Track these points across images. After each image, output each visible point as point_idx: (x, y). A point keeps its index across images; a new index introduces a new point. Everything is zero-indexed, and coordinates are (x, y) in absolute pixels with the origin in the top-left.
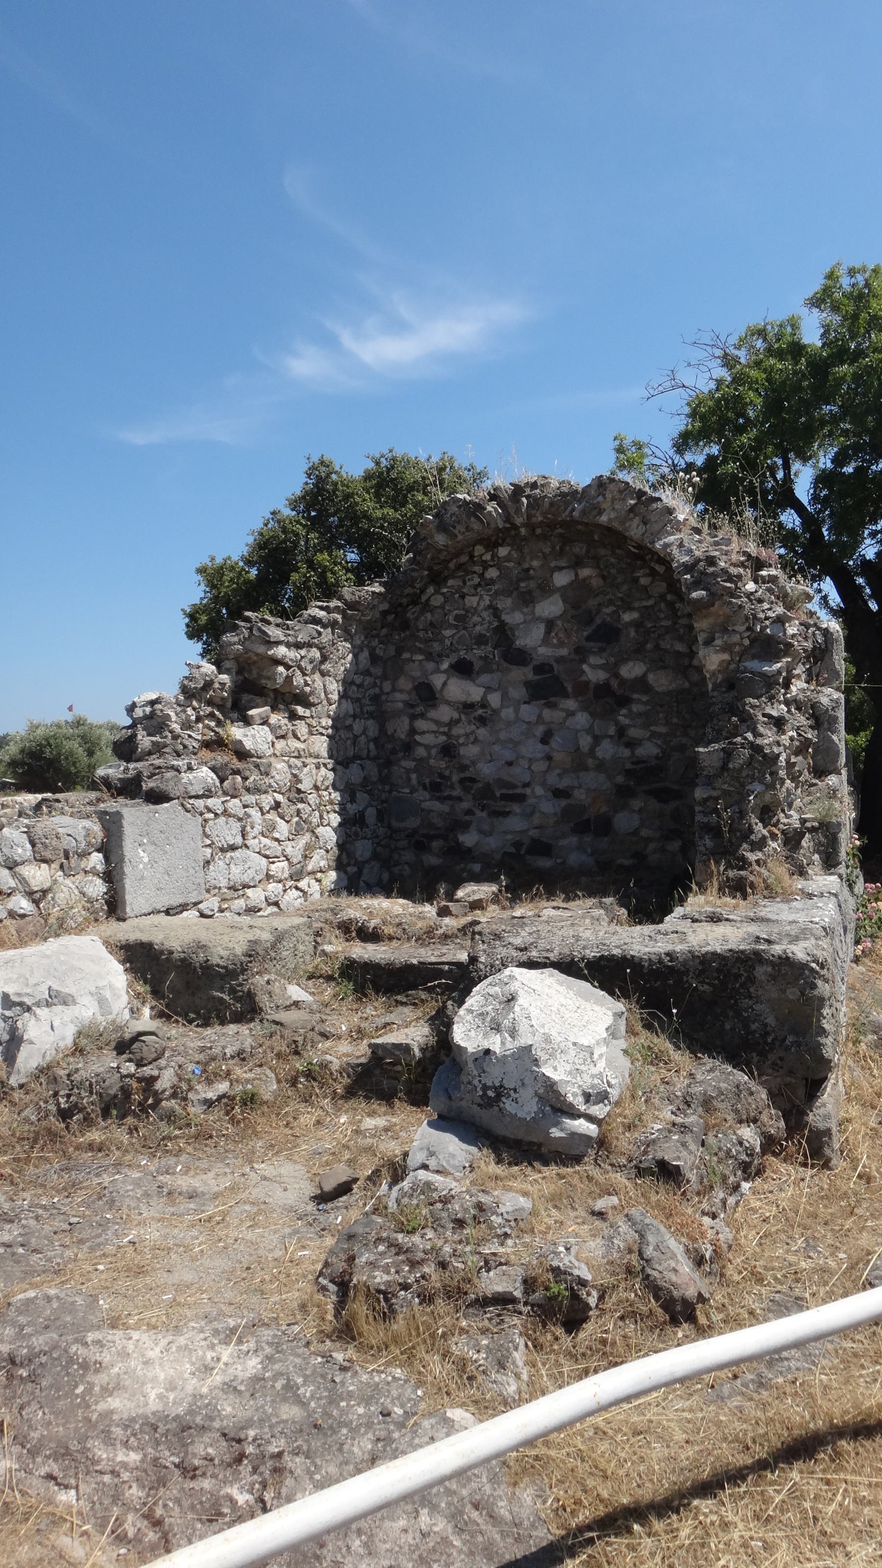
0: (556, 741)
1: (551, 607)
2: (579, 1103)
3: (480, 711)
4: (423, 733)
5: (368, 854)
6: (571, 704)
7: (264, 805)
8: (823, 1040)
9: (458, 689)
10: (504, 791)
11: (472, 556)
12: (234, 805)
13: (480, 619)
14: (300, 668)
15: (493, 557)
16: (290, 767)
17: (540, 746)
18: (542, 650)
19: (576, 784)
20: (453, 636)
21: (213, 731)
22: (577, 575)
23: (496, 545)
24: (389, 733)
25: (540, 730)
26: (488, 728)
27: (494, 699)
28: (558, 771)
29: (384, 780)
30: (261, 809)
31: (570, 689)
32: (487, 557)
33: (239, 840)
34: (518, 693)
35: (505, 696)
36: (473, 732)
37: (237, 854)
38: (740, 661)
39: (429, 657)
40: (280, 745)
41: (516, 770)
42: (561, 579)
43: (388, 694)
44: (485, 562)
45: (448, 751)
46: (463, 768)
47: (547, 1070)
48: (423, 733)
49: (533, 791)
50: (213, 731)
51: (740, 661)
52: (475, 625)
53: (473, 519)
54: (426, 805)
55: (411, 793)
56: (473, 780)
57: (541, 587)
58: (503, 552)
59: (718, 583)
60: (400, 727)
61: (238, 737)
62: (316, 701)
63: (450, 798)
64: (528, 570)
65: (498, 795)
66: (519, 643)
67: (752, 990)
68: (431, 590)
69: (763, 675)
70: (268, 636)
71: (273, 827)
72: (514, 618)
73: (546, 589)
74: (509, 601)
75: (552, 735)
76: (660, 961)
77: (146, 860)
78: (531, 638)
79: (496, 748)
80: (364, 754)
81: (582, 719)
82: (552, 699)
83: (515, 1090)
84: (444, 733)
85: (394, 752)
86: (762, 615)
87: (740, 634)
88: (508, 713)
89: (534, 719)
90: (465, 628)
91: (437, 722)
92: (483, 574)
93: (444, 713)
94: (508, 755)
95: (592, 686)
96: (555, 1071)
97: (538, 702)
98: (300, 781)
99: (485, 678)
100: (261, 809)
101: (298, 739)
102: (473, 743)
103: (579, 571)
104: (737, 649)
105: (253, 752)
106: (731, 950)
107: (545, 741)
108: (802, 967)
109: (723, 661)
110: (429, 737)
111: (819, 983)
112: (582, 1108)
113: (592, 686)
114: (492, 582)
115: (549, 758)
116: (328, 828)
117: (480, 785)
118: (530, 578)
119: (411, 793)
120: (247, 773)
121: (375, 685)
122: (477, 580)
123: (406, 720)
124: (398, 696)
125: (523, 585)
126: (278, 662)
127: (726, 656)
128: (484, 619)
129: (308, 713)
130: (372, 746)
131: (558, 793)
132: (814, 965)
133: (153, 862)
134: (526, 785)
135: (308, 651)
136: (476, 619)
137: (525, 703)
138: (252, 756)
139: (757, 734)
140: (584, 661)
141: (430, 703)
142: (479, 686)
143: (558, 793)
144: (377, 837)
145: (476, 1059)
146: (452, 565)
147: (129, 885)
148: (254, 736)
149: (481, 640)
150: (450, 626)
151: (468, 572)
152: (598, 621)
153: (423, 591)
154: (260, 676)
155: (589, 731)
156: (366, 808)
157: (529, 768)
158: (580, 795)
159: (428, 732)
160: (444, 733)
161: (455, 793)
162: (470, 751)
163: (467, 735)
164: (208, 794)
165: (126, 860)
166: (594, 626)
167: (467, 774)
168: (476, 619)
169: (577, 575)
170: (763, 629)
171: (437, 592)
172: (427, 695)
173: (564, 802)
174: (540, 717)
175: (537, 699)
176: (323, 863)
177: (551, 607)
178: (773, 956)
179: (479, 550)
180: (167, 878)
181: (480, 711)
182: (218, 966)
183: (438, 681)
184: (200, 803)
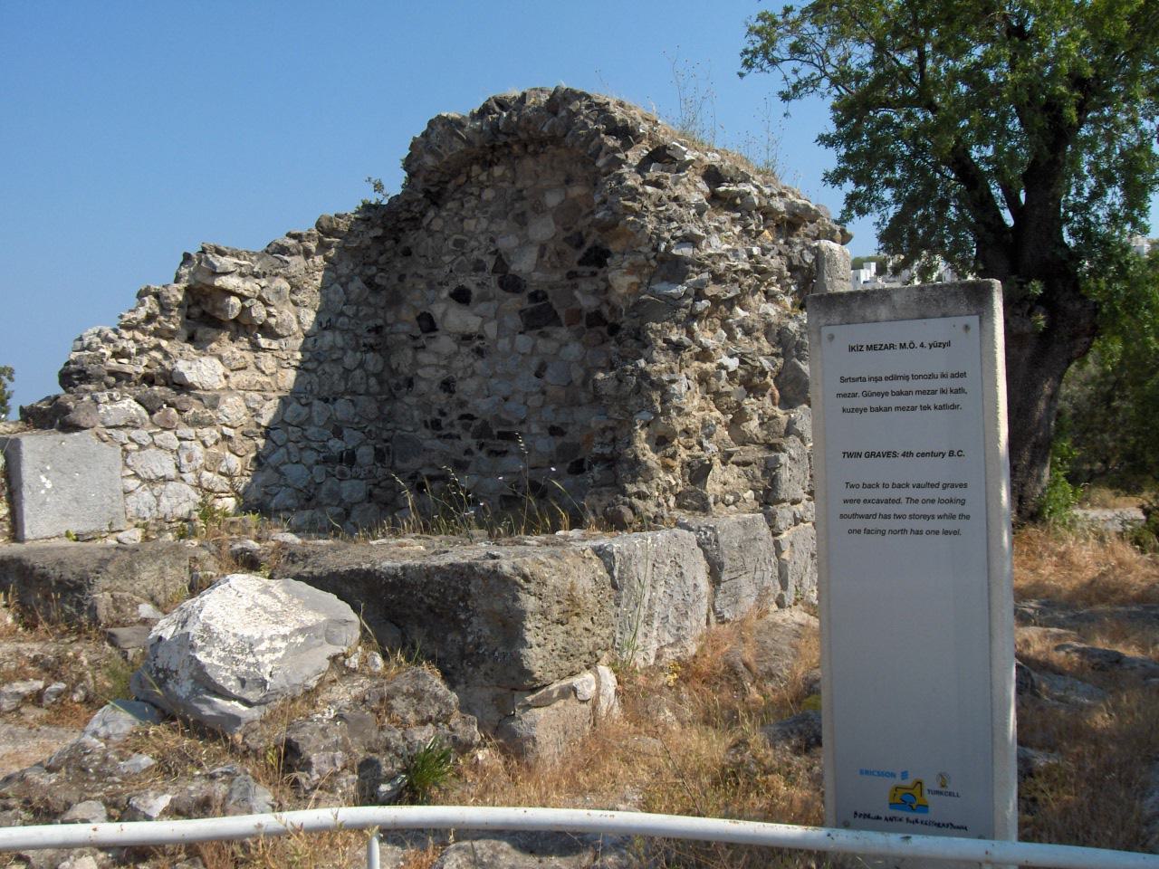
0: (550, 375)
1: (543, 229)
2: (232, 685)
3: (478, 343)
4: (426, 366)
5: (359, 496)
6: (563, 333)
7: (207, 438)
8: (525, 651)
9: (457, 319)
10: (501, 429)
11: (469, 177)
12: (169, 438)
13: (476, 244)
14: (260, 298)
15: (488, 175)
16: (245, 400)
17: (535, 379)
18: (537, 276)
19: (570, 421)
20: (452, 262)
21: (160, 364)
22: (566, 194)
23: (490, 164)
24: (394, 367)
25: (535, 362)
26: (485, 360)
27: (491, 330)
28: (553, 407)
29: (386, 418)
30: (204, 443)
31: (563, 319)
32: (483, 177)
33: (172, 472)
34: (514, 321)
35: (500, 327)
36: (471, 364)
37: (171, 486)
38: (649, 284)
39: (430, 286)
40: (237, 378)
41: (511, 406)
42: (553, 200)
43: (392, 325)
44: (482, 183)
45: (447, 386)
46: (462, 404)
47: (201, 656)
48: (426, 366)
49: (529, 428)
50: (160, 364)
51: (649, 284)
52: (472, 251)
53: (455, 139)
54: (428, 444)
55: (415, 431)
56: (470, 417)
57: (535, 209)
58: (497, 171)
59: (619, 202)
60: (403, 359)
61: (181, 370)
62: (286, 334)
63: (450, 436)
64: (521, 191)
65: (495, 432)
66: (514, 268)
67: (469, 603)
68: (431, 214)
69: (670, 297)
70: (215, 267)
71: (218, 460)
72: (507, 242)
73: (539, 209)
74: (504, 225)
75: (546, 368)
76: (396, 576)
77: (49, 485)
78: (524, 264)
79: (493, 381)
80: (362, 389)
81: (574, 350)
82: (547, 329)
83: (176, 672)
84: (444, 367)
85: (398, 387)
86: (667, 235)
87: (646, 255)
88: (504, 344)
89: (528, 350)
90: (463, 254)
91: (437, 354)
92: (480, 196)
93: (445, 344)
94: (504, 388)
95: (584, 314)
96: (208, 658)
97: (532, 332)
98: (259, 415)
99: (482, 307)
100: (204, 443)
101: (263, 372)
102: (471, 377)
103: (570, 191)
104: (646, 271)
105: (197, 385)
106: (451, 564)
107: (538, 375)
108: (503, 580)
109: (632, 284)
110: (430, 375)
111: (522, 595)
112: (236, 691)
113: (584, 314)
114: (488, 203)
115: (544, 393)
116: (300, 467)
117: (478, 423)
118: (523, 199)
119: (415, 431)
120: (185, 406)
121: (375, 315)
122: (474, 202)
123: (410, 353)
124: (400, 327)
125: (517, 205)
126: (231, 293)
127: (634, 279)
128: (481, 244)
129: (275, 345)
130: (373, 381)
131: (555, 431)
132: (518, 578)
133: (56, 489)
134: (523, 422)
135: (270, 282)
136: (473, 243)
137: (520, 333)
138: (197, 388)
139: (650, 361)
140: (575, 286)
141: (432, 334)
142: (476, 315)
143: (555, 431)
144: (375, 477)
145: (152, 645)
146: (450, 186)
147: (27, 508)
148: (199, 369)
149: (479, 266)
150: (448, 253)
151: (465, 193)
152: (588, 244)
153: (423, 215)
154: (215, 308)
155: (582, 362)
156: (359, 446)
157: (525, 403)
158: (574, 434)
159: (429, 365)
160: (444, 367)
161: (454, 432)
162: (468, 387)
163: (465, 368)
164: (132, 424)
165: (25, 484)
166: (584, 250)
167: (466, 411)
168: (473, 243)
169: (566, 194)
170: (668, 248)
171: (437, 215)
172: (428, 324)
173: (559, 440)
174: (534, 347)
175: (532, 328)
176: (290, 502)
177: (543, 229)
178: (483, 569)
179: (476, 169)
180: (75, 504)
181: (478, 343)
182: (69, 580)
183: (437, 310)
184: (122, 435)
